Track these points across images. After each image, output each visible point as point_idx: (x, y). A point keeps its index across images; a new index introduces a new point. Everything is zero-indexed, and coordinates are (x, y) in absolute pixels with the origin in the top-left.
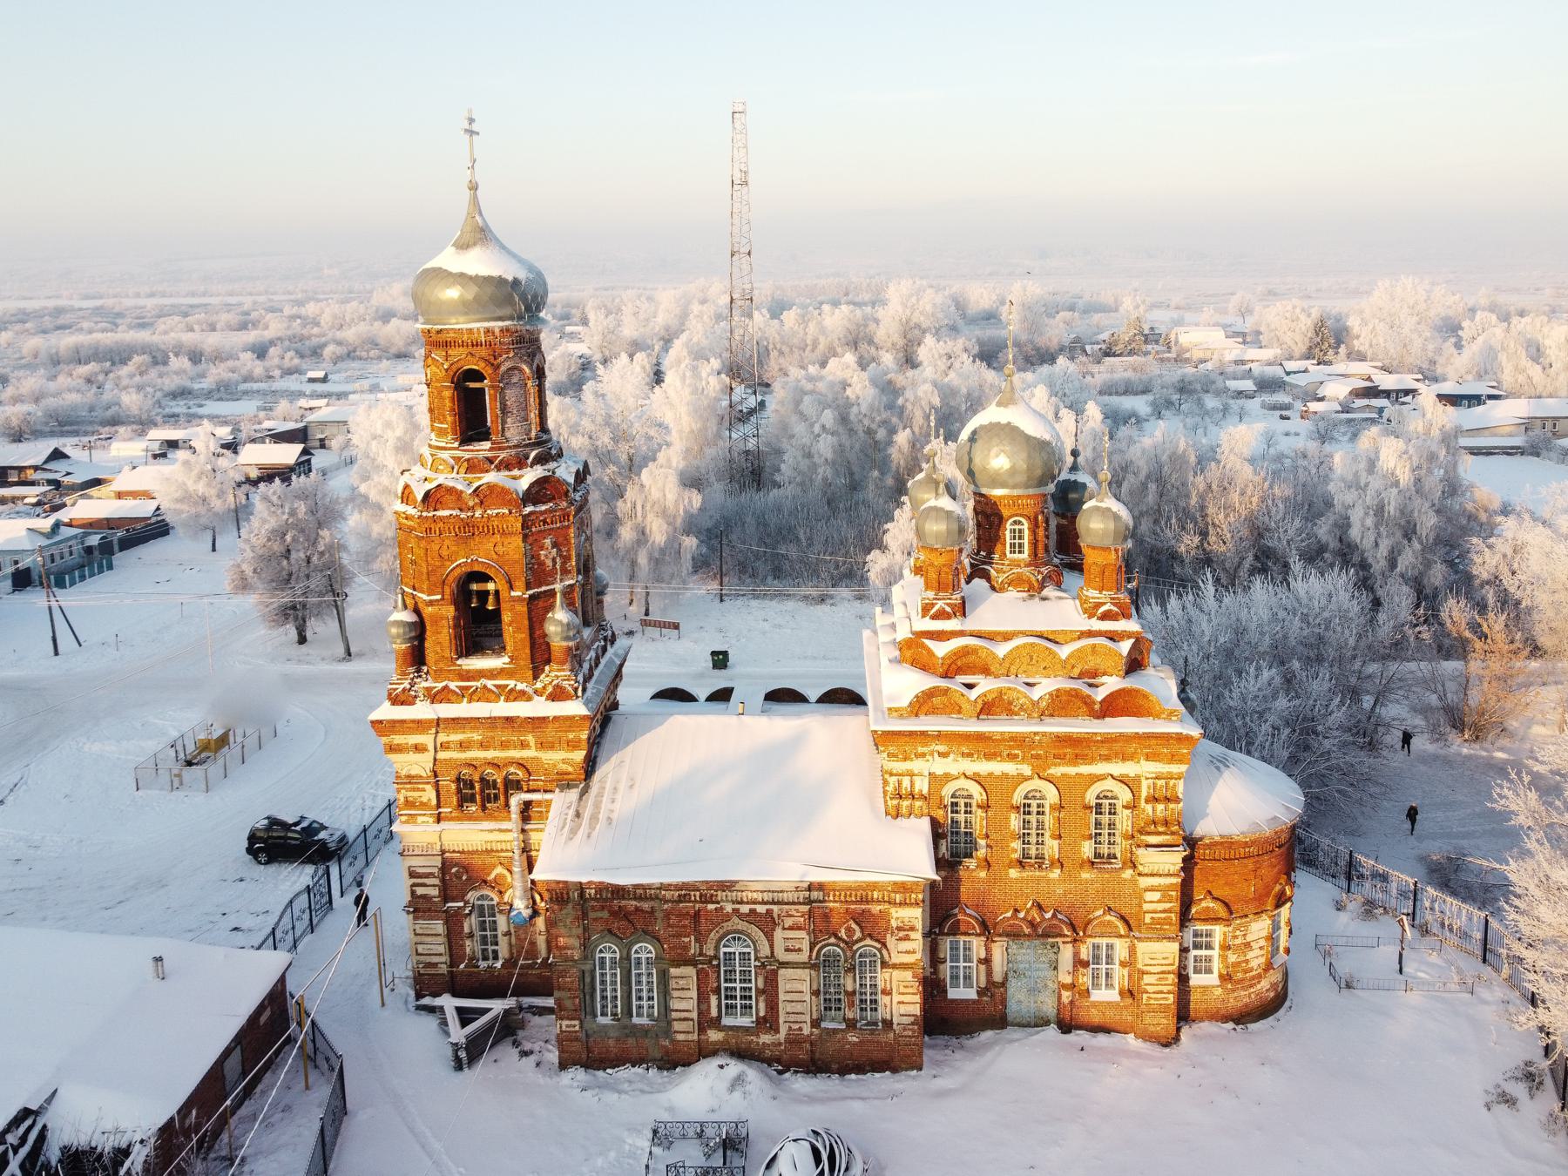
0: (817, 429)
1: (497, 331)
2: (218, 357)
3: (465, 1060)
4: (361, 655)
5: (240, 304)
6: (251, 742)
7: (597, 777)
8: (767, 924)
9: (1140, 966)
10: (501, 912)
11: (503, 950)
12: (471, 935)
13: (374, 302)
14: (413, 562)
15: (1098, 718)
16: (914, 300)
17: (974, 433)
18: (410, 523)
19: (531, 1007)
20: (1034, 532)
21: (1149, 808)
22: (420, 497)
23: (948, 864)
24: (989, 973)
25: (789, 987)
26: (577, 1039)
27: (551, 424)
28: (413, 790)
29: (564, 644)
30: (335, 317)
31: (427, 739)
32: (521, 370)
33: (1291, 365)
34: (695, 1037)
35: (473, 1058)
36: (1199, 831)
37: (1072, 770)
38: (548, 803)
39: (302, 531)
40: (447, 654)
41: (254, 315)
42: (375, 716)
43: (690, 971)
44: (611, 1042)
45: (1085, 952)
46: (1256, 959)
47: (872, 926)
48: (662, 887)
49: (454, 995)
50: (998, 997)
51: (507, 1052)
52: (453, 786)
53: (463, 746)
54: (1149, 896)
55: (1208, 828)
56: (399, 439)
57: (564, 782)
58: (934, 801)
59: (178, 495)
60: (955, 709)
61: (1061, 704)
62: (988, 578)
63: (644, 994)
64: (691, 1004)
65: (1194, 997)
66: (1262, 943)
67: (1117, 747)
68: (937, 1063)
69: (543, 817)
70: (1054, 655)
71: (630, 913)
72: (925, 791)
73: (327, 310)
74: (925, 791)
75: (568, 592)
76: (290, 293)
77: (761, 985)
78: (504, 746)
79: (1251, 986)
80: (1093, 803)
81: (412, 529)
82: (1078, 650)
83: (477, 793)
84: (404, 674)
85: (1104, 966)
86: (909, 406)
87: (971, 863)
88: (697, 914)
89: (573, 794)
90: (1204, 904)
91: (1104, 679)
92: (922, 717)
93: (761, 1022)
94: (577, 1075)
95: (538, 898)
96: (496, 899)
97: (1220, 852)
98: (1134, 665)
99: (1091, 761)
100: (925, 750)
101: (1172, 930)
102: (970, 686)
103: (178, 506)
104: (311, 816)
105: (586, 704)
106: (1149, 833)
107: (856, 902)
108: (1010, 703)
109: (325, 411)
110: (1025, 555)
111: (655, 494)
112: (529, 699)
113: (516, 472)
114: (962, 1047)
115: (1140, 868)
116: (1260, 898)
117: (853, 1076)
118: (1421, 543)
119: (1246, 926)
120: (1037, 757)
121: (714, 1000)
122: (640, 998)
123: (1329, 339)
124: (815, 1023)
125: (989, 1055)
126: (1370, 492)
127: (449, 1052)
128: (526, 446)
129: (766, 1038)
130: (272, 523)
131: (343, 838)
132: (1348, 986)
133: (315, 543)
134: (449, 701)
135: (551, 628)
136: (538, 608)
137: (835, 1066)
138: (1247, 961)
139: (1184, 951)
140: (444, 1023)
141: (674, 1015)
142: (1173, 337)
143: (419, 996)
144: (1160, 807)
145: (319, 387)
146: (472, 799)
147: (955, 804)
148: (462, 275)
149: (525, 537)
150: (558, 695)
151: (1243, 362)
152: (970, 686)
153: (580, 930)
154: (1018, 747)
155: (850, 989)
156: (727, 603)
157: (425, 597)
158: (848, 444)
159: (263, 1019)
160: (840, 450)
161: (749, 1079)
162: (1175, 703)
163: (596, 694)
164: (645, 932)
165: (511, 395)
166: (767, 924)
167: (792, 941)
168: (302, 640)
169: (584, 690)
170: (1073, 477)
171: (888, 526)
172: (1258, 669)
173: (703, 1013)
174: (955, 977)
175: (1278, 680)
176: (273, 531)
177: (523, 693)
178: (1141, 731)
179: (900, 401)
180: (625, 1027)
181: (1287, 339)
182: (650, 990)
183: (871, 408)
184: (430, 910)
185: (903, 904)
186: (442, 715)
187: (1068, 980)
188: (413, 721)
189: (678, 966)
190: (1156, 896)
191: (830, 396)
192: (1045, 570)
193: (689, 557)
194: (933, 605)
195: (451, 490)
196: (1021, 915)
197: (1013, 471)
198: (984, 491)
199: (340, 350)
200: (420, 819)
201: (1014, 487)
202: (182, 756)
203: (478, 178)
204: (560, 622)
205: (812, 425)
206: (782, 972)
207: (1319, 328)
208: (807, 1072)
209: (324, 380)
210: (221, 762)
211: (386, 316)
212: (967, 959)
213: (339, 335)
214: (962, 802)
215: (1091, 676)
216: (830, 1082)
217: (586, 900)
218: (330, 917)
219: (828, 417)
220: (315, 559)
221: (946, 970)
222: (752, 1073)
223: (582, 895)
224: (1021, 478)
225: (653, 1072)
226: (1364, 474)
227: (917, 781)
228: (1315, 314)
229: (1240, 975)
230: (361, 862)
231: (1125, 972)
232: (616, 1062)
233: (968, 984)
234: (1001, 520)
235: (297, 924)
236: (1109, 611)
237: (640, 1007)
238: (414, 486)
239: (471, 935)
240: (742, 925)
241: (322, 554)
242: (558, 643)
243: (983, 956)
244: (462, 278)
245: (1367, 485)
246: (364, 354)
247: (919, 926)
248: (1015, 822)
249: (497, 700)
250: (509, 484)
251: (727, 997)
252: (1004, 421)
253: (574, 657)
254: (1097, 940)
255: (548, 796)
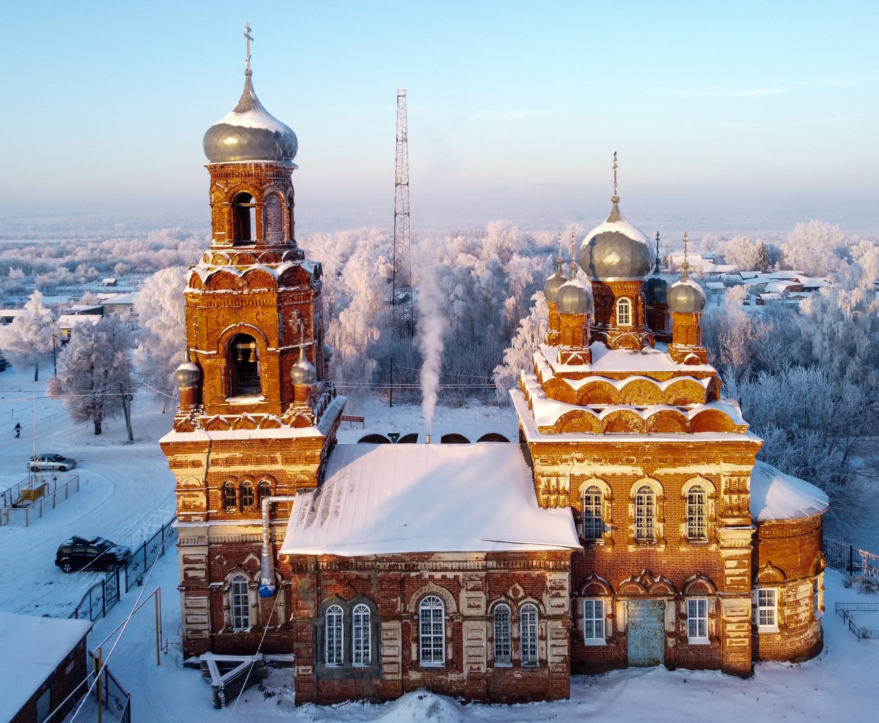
0: (452, 297)
1: (263, 166)
2: (43, 270)
3: (223, 700)
4: (140, 440)
5: (58, 244)
6: (61, 493)
7: (326, 485)
8: (454, 587)
9: (724, 617)
10: (252, 588)
11: (252, 619)
12: (228, 608)
13: (149, 240)
14: (197, 328)
15: (688, 432)
16: (505, 232)
17: (594, 239)
18: (196, 300)
19: (272, 662)
20: (635, 306)
21: (727, 498)
22: (204, 280)
23: (587, 540)
24: (615, 625)
25: (470, 635)
26: (310, 681)
27: (296, 238)
28: (190, 496)
29: (305, 385)
30: (122, 249)
31: (201, 457)
32: (279, 195)
33: (745, 274)
34: (400, 677)
35: (229, 700)
36: (761, 517)
37: (671, 471)
38: (292, 502)
39: (103, 353)
40: (219, 394)
41: (68, 248)
42: (163, 440)
43: (396, 624)
44: (336, 683)
45: (684, 608)
46: (803, 613)
47: (536, 588)
48: (379, 559)
49: (214, 652)
50: (621, 645)
51: (255, 695)
52: (220, 493)
53: (228, 462)
54: (729, 564)
55: (767, 514)
56: (174, 289)
57: (302, 488)
58: (574, 495)
59: (14, 340)
60: (587, 427)
61: (662, 423)
62: (605, 340)
63: (362, 645)
64: (397, 651)
65: (762, 642)
66: (807, 601)
67: (703, 453)
68: (579, 694)
69: (286, 515)
70: (657, 388)
71: (352, 580)
72: (567, 488)
73: (117, 245)
74: (567, 488)
75: (308, 350)
76: (92, 237)
77: (449, 634)
78: (259, 461)
79: (801, 634)
80: (687, 495)
81: (196, 305)
82: (673, 385)
83: (238, 497)
84: (186, 409)
85: (698, 618)
86: (512, 283)
87: (601, 542)
88: (402, 582)
89: (309, 497)
90: (766, 572)
91: (692, 405)
92: (565, 434)
93: (449, 663)
94: (309, 709)
95: (279, 577)
96: (248, 579)
97: (776, 532)
98: (711, 397)
99: (685, 463)
100: (567, 457)
101: (745, 589)
102: (598, 411)
103: (13, 348)
104: (106, 537)
105: (320, 429)
106: (728, 517)
107: (520, 569)
108: (627, 422)
109: (112, 298)
110: (630, 324)
111: (349, 329)
112: (278, 426)
113: (273, 264)
114: (597, 682)
115: (722, 543)
116: (805, 567)
117: (518, 705)
118: (860, 357)
119: (796, 587)
120: (647, 461)
121: (414, 647)
122: (358, 648)
123: (769, 259)
124: (490, 664)
125: (618, 687)
126: (826, 325)
127: (210, 695)
128: (281, 247)
129: (453, 677)
130: (81, 348)
131: (128, 552)
132: (865, 637)
133: (112, 361)
134: (219, 429)
135: (296, 375)
136: (286, 360)
137: (504, 698)
138: (797, 615)
139: (754, 606)
140: (207, 675)
141: (384, 659)
142: (669, 259)
143: (186, 656)
144: (735, 497)
145: (111, 288)
146: (233, 503)
147: (588, 498)
148: (240, 128)
149: (279, 309)
150: (300, 423)
151: (715, 273)
152: (598, 411)
153: (315, 595)
154: (634, 454)
155: (515, 635)
156: (395, 408)
157: (204, 352)
158: (472, 307)
159: (68, 670)
160: (467, 311)
161: (441, 707)
162: (741, 422)
163: (327, 424)
164: (364, 595)
165: (272, 212)
166: (454, 587)
167: (471, 601)
168: (98, 431)
169: (318, 421)
170: (656, 277)
171: (507, 350)
172: (770, 429)
173: (406, 658)
174: (589, 630)
175: (785, 436)
176: (82, 353)
177: (274, 422)
178: (720, 440)
179: (507, 280)
180: (347, 670)
181: (742, 259)
182: (366, 641)
183: (488, 283)
184: (198, 588)
185: (555, 569)
186: (214, 439)
187: (672, 629)
188: (192, 443)
189: (387, 621)
190: (734, 563)
191: (460, 277)
192: (644, 334)
193: (370, 373)
194: (570, 355)
195: (227, 275)
196: (638, 580)
197: (621, 264)
198: (601, 279)
199: (125, 267)
200: (194, 518)
201: (621, 276)
202: (9, 503)
203: (252, 68)
204: (302, 370)
205: (449, 295)
206: (465, 624)
207: (763, 250)
208: (484, 702)
209: (115, 284)
210: (37, 505)
211: (157, 248)
212: (599, 615)
213: (125, 258)
214: (593, 496)
215: (683, 403)
216: (501, 710)
217: (320, 571)
218: (117, 607)
219: (460, 289)
220: (111, 372)
221: (583, 623)
222: (444, 703)
223: (317, 566)
224: (627, 269)
225: (367, 706)
226: (820, 314)
227: (561, 480)
228: (759, 243)
229: (793, 625)
230: (141, 569)
231: (713, 622)
232: (339, 699)
233: (599, 635)
234: (613, 299)
235: (94, 609)
236: (693, 358)
237: (358, 655)
238: (200, 273)
239: (228, 608)
240: (436, 588)
241: (116, 369)
242: (300, 385)
243: (610, 612)
244: (239, 130)
245: (823, 320)
246: (141, 269)
247: (567, 585)
248: (631, 510)
249: (254, 427)
250: (269, 271)
251: (423, 646)
252: (614, 231)
253: (311, 396)
254: (692, 599)
255: (291, 499)
